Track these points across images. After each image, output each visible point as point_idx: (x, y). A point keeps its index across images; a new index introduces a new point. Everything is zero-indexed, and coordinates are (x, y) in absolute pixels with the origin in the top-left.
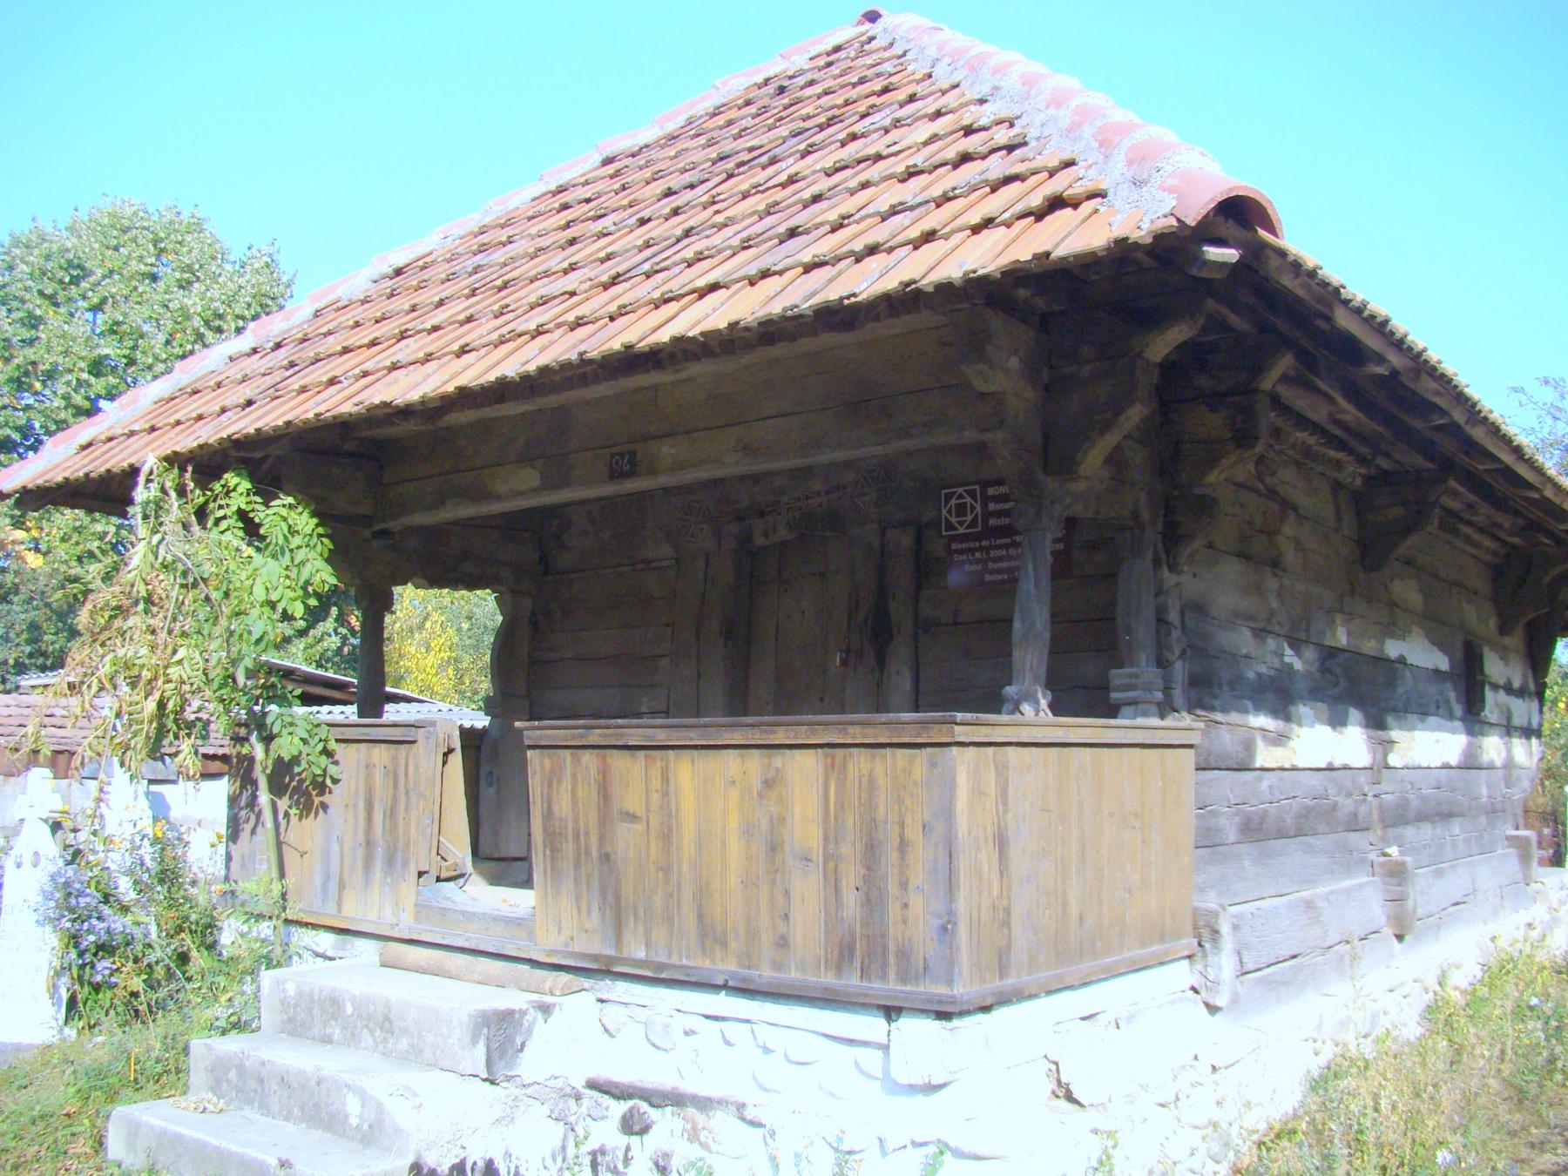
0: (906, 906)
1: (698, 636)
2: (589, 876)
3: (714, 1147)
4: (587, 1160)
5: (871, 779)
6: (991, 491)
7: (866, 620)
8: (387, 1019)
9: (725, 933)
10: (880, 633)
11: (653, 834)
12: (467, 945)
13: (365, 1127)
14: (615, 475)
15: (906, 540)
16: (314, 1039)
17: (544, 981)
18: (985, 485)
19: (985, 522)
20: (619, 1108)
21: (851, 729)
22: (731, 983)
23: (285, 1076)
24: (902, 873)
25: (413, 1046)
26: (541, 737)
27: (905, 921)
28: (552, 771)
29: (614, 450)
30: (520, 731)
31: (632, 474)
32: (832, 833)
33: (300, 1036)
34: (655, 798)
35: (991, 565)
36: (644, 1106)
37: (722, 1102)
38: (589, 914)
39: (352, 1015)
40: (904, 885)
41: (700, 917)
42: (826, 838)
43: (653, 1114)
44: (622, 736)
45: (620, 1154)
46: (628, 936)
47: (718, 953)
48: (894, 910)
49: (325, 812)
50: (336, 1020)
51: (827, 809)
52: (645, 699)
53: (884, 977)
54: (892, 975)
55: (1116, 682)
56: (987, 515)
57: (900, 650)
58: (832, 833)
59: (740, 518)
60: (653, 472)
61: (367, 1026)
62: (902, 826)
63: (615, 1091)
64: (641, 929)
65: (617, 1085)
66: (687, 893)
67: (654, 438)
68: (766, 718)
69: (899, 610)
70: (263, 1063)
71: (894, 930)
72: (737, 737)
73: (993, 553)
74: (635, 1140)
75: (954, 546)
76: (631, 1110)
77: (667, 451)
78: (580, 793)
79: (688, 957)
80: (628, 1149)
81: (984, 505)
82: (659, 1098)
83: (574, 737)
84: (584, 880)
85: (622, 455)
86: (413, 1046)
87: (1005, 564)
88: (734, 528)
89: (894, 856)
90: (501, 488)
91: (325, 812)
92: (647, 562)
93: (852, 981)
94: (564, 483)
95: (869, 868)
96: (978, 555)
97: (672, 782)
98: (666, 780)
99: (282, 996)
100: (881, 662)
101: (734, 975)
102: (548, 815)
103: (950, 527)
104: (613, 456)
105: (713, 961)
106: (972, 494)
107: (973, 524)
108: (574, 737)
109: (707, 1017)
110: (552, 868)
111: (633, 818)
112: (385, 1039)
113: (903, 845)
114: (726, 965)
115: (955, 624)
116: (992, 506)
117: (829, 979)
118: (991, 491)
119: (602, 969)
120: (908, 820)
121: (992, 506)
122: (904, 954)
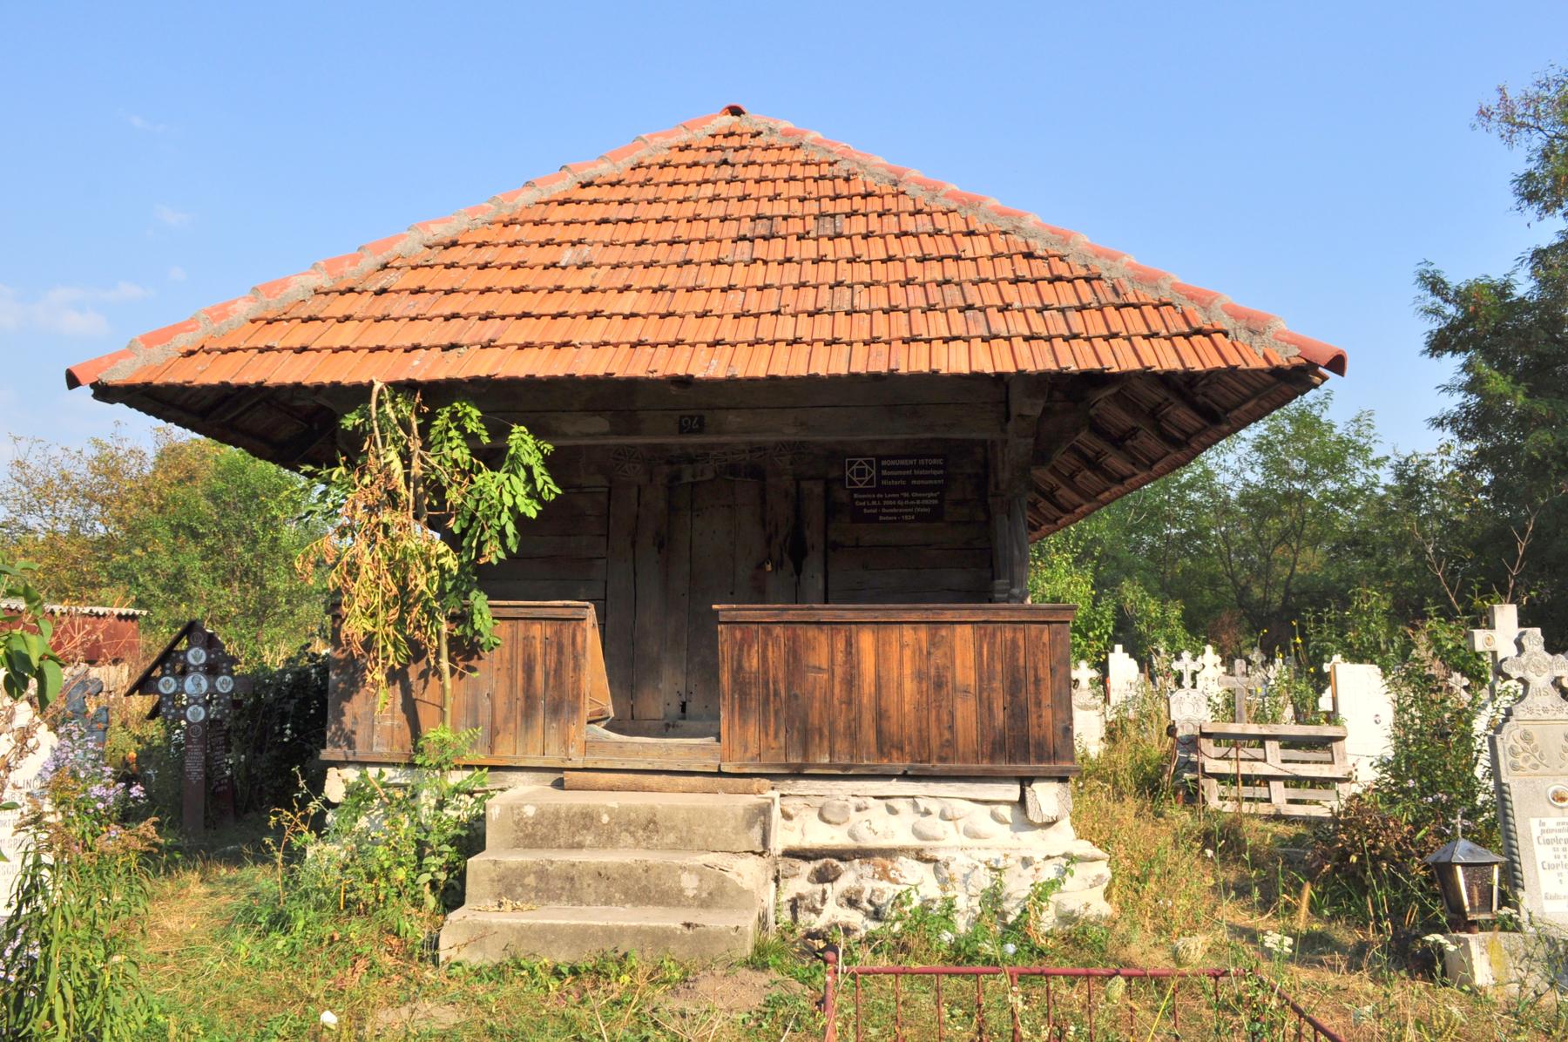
0: (1040, 716)
1: (633, 544)
2: (776, 713)
3: (901, 880)
4: (787, 906)
5: (1014, 641)
6: (884, 463)
7: (785, 541)
8: (652, 821)
9: (901, 742)
10: (798, 553)
11: (837, 680)
12: (650, 767)
13: (704, 895)
14: (683, 430)
15: (818, 489)
16: (559, 847)
17: (750, 785)
18: (879, 458)
19: (879, 482)
20: (807, 868)
21: (1002, 613)
22: (910, 773)
23: (603, 872)
24: (1037, 698)
25: (681, 839)
26: (736, 616)
27: (1039, 726)
28: (742, 639)
29: (682, 413)
30: (717, 611)
31: (701, 429)
32: (985, 677)
33: (541, 847)
34: (840, 657)
35: (884, 510)
36: (835, 862)
37: (903, 851)
38: (776, 736)
39: (608, 824)
40: (1039, 704)
41: (879, 732)
42: (981, 679)
43: (842, 865)
44: (798, 615)
45: (818, 897)
46: (813, 749)
47: (895, 754)
48: (1033, 720)
49: (460, 678)
50: (588, 829)
51: (982, 661)
52: (583, 590)
53: (1027, 760)
54: (1032, 759)
55: (998, 588)
56: (880, 477)
57: (813, 565)
58: (985, 677)
59: (670, 462)
60: (719, 432)
61: (627, 830)
62: (1036, 670)
63: (809, 854)
64: (826, 744)
65: (811, 850)
66: (868, 718)
67: (720, 408)
68: (939, 605)
69: (813, 536)
70: (573, 865)
71: (1034, 732)
72: (914, 617)
73: (885, 503)
74: (827, 886)
75: (856, 496)
76: (825, 865)
77: (733, 419)
78: (770, 654)
79: (868, 759)
80: (824, 892)
81: (879, 472)
82: (843, 855)
83: (769, 616)
84: (772, 714)
85: (692, 418)
86: (681, 839)
87: (895, 510)
88: (666, 469)
89: (1031, 688)
90: (569, 429)
91: (460, 678)
92: (579, 487)
93: (1002, 766)
94: (634, 430)
95: (1012, 695)
96: (874, 503)
97: (854, 646)
98: (849, 643)
99: (517, 818)
100: (798, 570)
101: (911, 768)
102: (738, 670)
103: (851, 483)
104: (682, 417)
105: (890, 760)
106: (870, 464)
107: (870, 482)
108: (769, 616)
109: (875, 797)
110: (740, 707)
111: (820, 669)
112: (648, 837)
113: (1037, 681)
114: (899, 765)
115: (857, 546)
116: (884, 473)
117: (985, 765)
118: (884, 463)
119: (798, 774)
120: (1040, 665)
121: (884, 473)
122: (1040, 745)
